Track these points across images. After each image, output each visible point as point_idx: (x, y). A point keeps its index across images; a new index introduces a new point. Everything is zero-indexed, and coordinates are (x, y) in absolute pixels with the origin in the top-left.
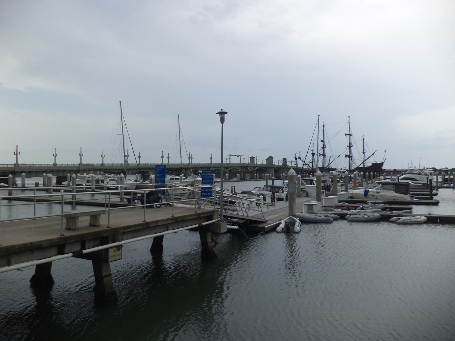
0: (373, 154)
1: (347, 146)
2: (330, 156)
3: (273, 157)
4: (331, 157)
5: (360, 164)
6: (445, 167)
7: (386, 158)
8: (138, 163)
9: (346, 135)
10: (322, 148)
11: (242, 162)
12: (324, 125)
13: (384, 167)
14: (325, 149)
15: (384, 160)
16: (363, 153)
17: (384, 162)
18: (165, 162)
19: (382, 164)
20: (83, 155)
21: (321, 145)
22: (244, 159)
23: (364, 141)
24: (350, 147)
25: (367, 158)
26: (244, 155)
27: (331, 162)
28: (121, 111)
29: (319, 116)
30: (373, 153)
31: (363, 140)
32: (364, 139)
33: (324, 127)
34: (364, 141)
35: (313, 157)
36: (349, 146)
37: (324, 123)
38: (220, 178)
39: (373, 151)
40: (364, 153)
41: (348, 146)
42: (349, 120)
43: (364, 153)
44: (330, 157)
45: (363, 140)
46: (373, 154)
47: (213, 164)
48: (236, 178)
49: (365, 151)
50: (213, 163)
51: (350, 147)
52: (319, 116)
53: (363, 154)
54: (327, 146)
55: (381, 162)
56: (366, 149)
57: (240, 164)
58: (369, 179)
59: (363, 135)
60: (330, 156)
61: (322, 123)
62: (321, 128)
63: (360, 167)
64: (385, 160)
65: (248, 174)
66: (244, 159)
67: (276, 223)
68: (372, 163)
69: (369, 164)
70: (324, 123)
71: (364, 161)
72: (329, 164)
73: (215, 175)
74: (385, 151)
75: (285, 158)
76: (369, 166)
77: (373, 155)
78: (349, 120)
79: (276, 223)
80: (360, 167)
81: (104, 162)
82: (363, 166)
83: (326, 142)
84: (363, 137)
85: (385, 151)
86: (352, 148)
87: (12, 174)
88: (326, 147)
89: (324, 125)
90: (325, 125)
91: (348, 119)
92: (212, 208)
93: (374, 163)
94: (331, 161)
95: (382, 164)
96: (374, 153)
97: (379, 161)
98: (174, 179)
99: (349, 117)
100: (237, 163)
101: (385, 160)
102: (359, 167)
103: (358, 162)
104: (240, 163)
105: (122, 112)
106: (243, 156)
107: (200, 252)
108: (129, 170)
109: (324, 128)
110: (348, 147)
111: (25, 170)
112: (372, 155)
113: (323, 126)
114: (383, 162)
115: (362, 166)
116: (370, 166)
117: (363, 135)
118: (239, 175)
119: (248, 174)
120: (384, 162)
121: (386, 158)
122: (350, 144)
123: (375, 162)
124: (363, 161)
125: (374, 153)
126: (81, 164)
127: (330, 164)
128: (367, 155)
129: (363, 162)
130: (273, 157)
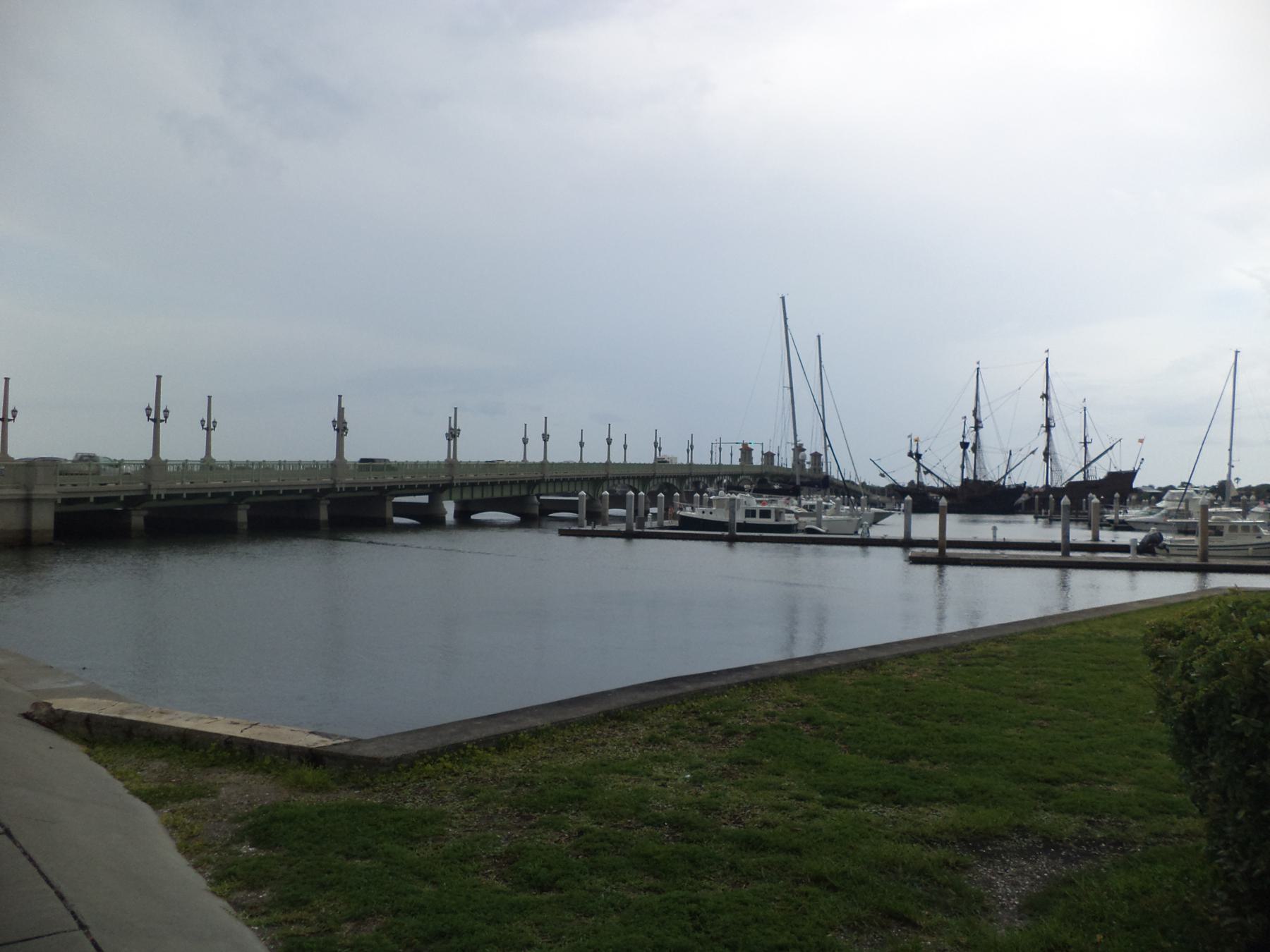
0: (1111, 448)
1: (1040, 426)
2: (1010, 452)
3: (752, 450)
4: (1012, 453)
5: (1075, 473)
6: (1147, 485)
7: (1143, 459)
8: (780, 465)
9: (1042, 397)
10: (973, 429)
11: (535, 457)
12: (978, 369)
13: (1137, 484)
14: (981, 431)
15: (1138, 463)
16: (1083, 444)
17: (1139, 468)
18: (617, 458)
19: (1132, 475)
20: (215, 427)
21: (971, 422)
22: (545, 437)
24: (1048, 427)
25: (1092, 460)
27: (1013, 466)
28: (786, 323)
29: (1237, 352)
30: (1111, 445)
31: (1085, 410)
32: (1087, 408)
35: (964, 454)
37: (978, 363)
38: (656, 506)
39: (1111, 441)
40: (1085, 443)
41: (1042, 426)
42: (1047, 359)
43: (1085, 443)
44: (1010, 454)
45: (1085, 410)
46: (1111, 448)
47: (553, 464)
48: (623, 508)
50: (462, 457)
51: (1048, 427)
52: (1237, 352)
53: (1084, 448)
55: (1129, 468)
56: (1091, 435)
57: (524, 465)
59: (1085, 400)
60: (1010, 452)
62: (973, 376)
63: (1074, 480)
64: (1141, 463)
66: (545, 437)
68: (1108, 470)
69: (1099, 472)
70: (978, 363)
71: (1086, 466)
74: (1141, 441)
75: (816, 452)
76: (1098, 479)
77: (1110, 452)
78: (1047, 359)
80: (1074, 482)
81: (722, 462)
82: (1082, 479)
83: (983, 415)
84: (1084, 405)
85: (1141, 441)
86: (1053, 431)
87: (946, 497)
88: (982, 427)
89: (978, 369)
90: (980, 370)
91: (1046, 355)
93: (1113, 470)
94: (1012, 466)
95: (1132, 475)
96: (1113, 446)
97: (1126, 467)
98: (758, 514)
99: (1048, 351)
100: (422, 458)
101: (1141, 463)
102: (1073, 481)
103: (1069, 469)
104: (519, 459)
105: (789, 328)
106: (760, 446)
107: (735, 738)
108: (582, 481)
109: (980, 376)
110: (1044, 429)
111: (368, 483)
112: (1108, 450)
113: (976, 372)
114: (1136, 469)
115: (1080, 478)
116: (1100, 480)
117: (1085, 400)
120: (1139, 468)
121: (1143, 459)
122: (1048, 420)
123: (1115, 468)
124: (1083, 466)
125: (1113, 446)
126: (451, 464)
127: (1011, 470)
129: (1083, 469)
130: (752, 450)
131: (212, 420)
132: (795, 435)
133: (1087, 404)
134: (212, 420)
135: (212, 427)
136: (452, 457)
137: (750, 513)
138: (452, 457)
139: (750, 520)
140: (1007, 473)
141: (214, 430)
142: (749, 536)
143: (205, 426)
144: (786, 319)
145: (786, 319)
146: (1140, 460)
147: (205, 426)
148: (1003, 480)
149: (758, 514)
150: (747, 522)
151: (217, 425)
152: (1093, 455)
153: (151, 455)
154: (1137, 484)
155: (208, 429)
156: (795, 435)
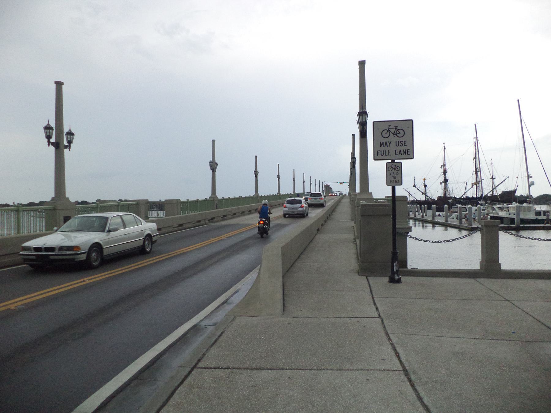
0: (504, 181)
2: (466, 183)
15: (516, 187)
19: (515, 191)
20: (70, 142)
23: (492, 166)
24: (476, 172)
26: (396, 155)
30: (504, 179)
31: (492, 164)
32: (493, 163)
33: (444, 149)
34: (492, 166)
36: (475, 172)
40: (493, 178)
41: (474, 172)
44: (466, 184)
46: (504, 181)
49: (494, 177)
54: (448, 171)
58: (448, 209)
61: (443, 144)
63: (489, 195)
64: (517, 187)
65: (424, 205)
67: (133, 202)
69: (499, 191)
71: (493, 189)
72: (465, 193)
73: (435, 205)
77: (504, 182)
79: (133, 202)
84: (491, 161)
89: (444, 146)
90: (446, 147)
92: (179, 251)
95: (515, 191)
96: (505, 179)
97: (511, 189)
98: (542, 214)
101: (517, 187)
104: (205, 194)
110: (475, 173)
118: (426, 206)
119: (424, 205)
121: (518, 185)
125: (505, 179)
128: (497, 182)
131: (66, 130)
132: (528, 172)
133: (493, 161)
134: (66, 130)
135: (66, 143)
136: (358, 190)
137: (538, 213)
138: (358, 190)
139: (539, 217)
140: (465, 193)
141: (69, 147)
142: (535, 226)
143: (53, 140)
144: (520, 111)
145: (520, 111)
146: (517, 186)
147: (53, 140)
148: (463, 196)
149: (542, 214)
150: (538, 218)
151: (74, 141)
152: (496, 184)
153: (73, 199)
154: (518, 194)
155: (57, 146)
156: (528, 172)
